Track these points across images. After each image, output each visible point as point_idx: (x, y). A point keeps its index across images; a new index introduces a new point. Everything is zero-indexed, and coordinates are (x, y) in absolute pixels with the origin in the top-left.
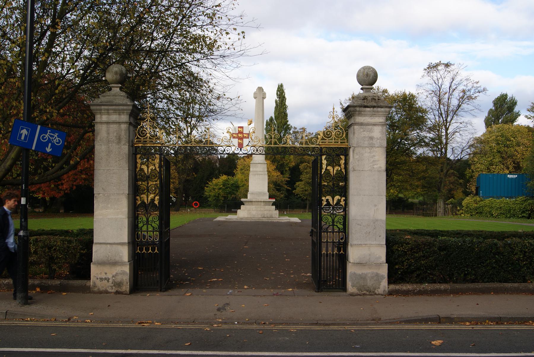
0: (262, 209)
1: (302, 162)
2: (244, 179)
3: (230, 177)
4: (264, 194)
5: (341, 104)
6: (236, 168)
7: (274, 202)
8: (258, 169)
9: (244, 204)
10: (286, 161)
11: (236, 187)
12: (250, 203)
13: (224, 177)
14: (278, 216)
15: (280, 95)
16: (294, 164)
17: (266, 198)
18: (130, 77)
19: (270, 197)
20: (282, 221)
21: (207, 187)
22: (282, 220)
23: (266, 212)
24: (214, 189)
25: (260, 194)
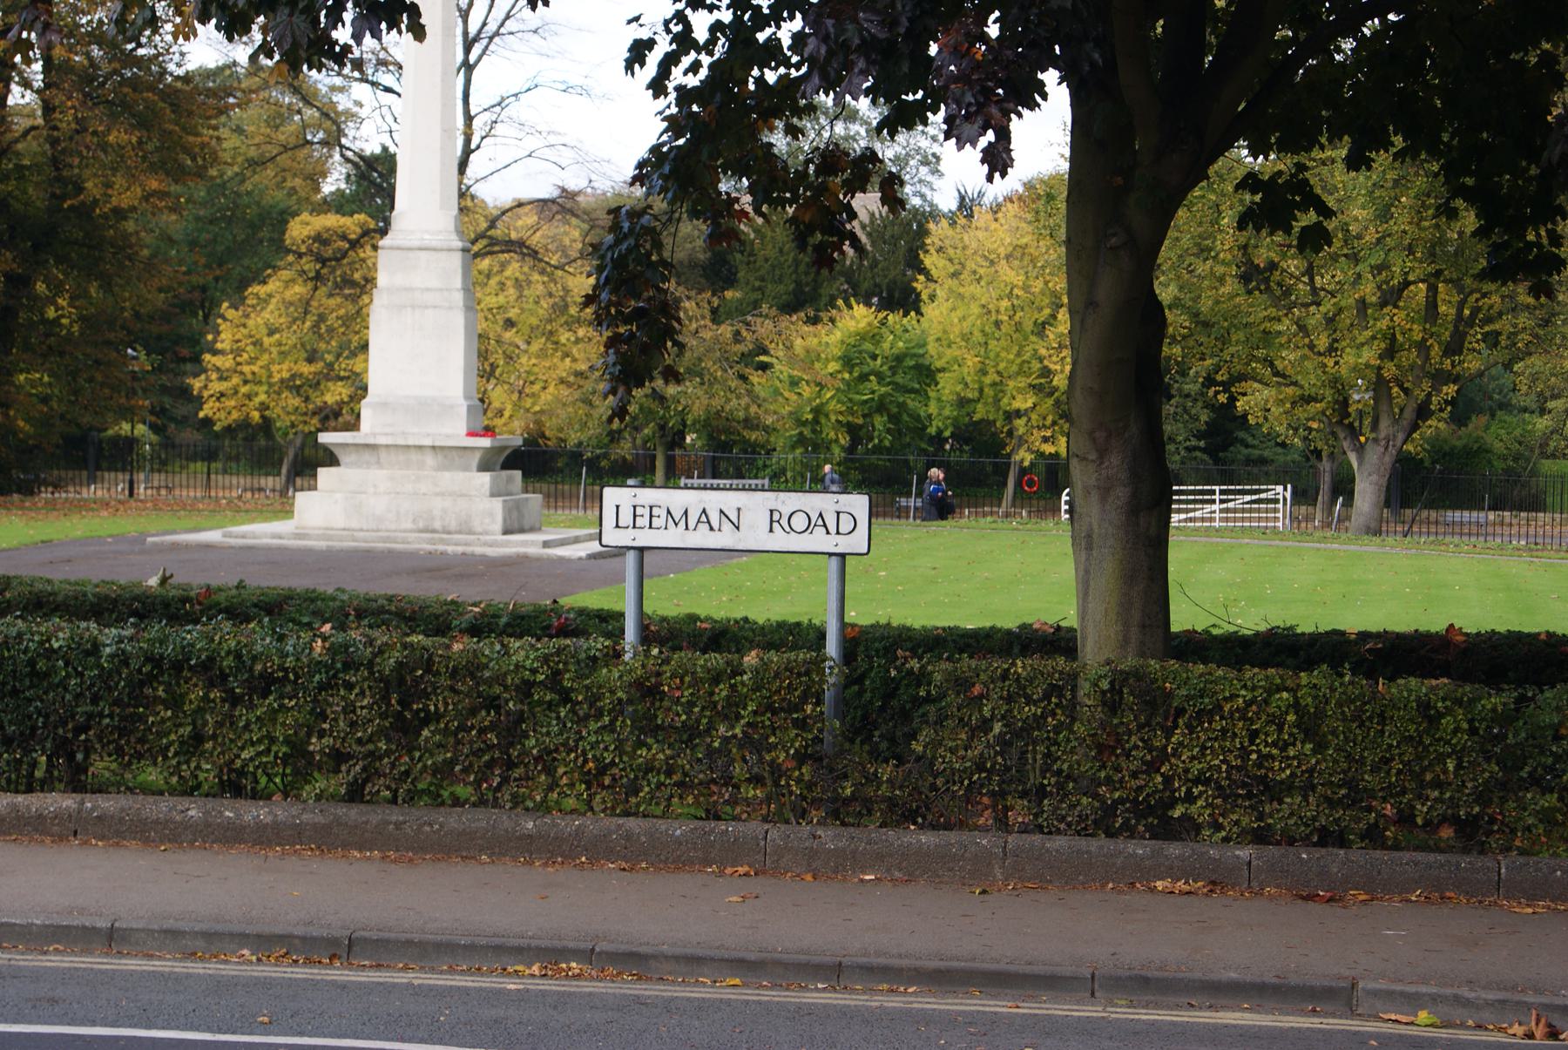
23: (438, 505)
25: (423, 408)
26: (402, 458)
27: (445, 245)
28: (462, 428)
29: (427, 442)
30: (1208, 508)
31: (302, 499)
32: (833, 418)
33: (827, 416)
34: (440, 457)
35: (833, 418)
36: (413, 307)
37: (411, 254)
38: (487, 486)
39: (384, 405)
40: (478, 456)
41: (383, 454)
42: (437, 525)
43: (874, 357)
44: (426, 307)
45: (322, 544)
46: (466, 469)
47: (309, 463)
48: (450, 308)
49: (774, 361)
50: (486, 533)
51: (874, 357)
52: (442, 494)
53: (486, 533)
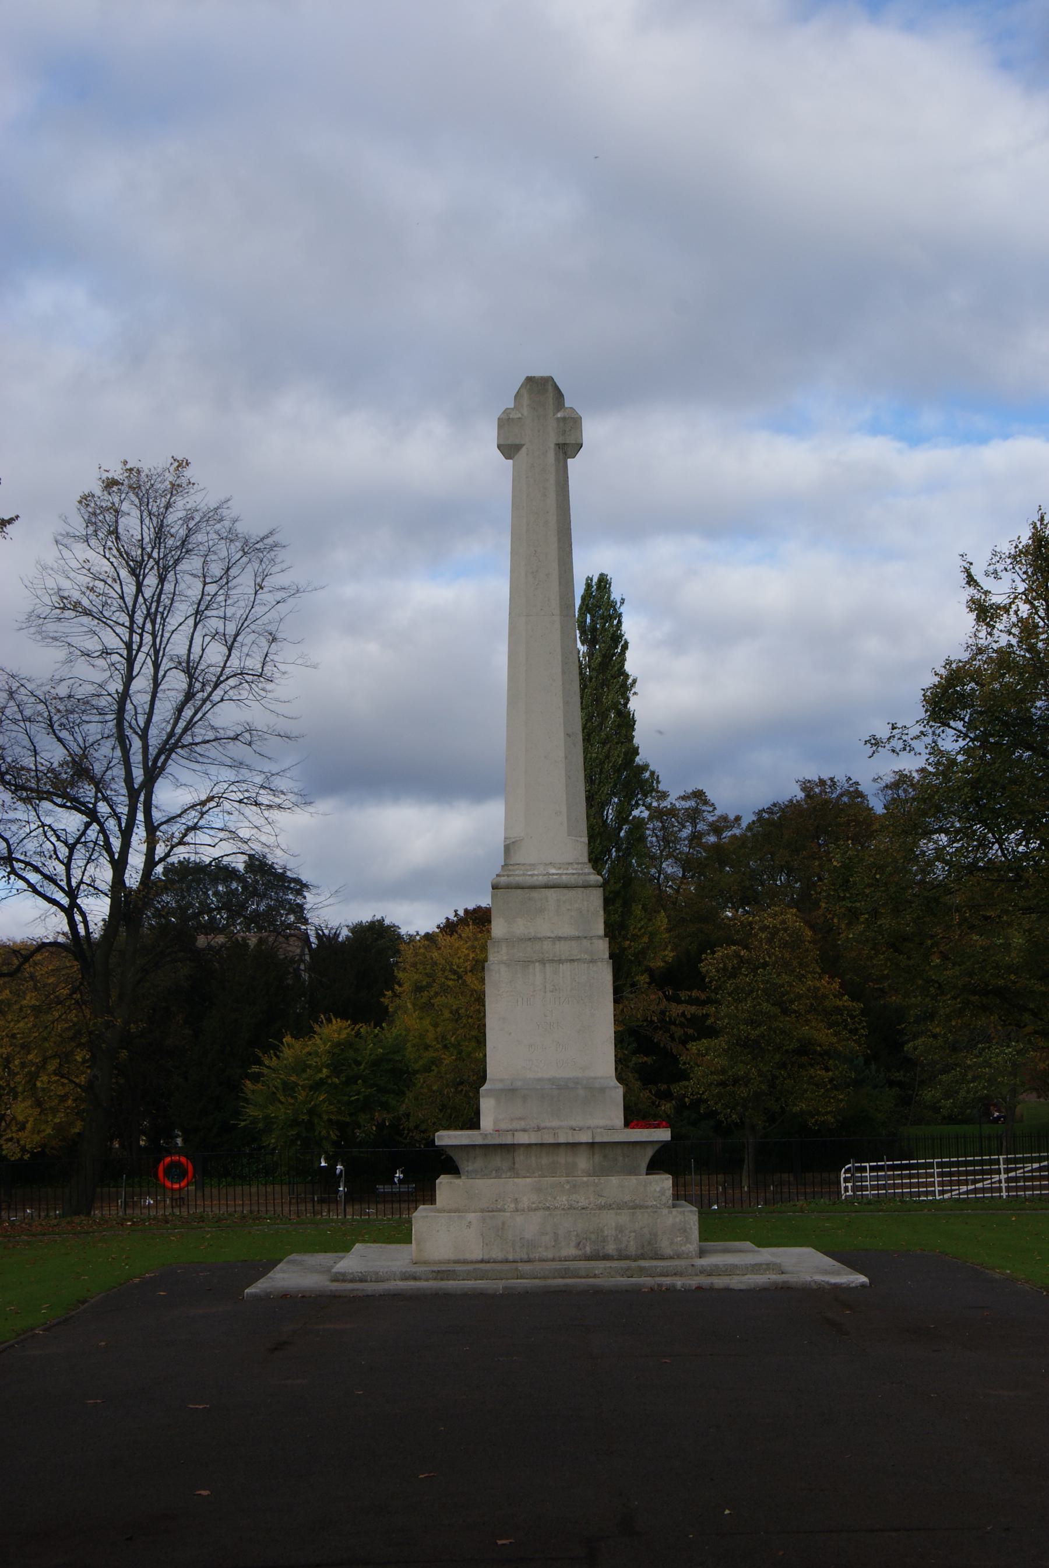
0: (581, 1200)
1: (709, 945)
2: (431, 1035)
3: (364, 1029)
4: (594, 1092)
5: (971, 581)
6: (390, 981)
7: (664, 1146)
8: (543, 927)
9: (454, 1170)
10: (635, 938)
11: (394, 1073)
12: (497, 1161)
13: (334, 1030)
14: (693, 1246)
15: (594, 629)
16: (670, 954)
17: (607, 1119)
18: (177, 902)
19: (633, 1116)
20: (735, 1282)
21: (256, 1078)
22: (729, 1270)
23: (610, 1221)
24: (289, 1088)
25: (564, 1092)
26: (545, 1161)
27: (580, 881)
28: (617, 1117)
29: (585, 1138)
30: (996, 1178)
31: (422, 1218)
32: (325, 1117)
33: (320, 1117)
34: (598, 1158)
35: (325, 1117)
36: (543, 962)
37: (535, 894)
38: (669, 1193)
39: (510, 1093)
40: (650, 1153)
41: (520, 1158)
42: (611, 1248)
43: (358, 1063)
44: (560, 961)
45: (497, 1286)
46: (633, 1171)
47: (429, 1168)
48: (593, 961)
49: (265, 1071)
50: (679, 1256)
51: (358, 1063)
52: (608, 1207)
53: (679, 1256)
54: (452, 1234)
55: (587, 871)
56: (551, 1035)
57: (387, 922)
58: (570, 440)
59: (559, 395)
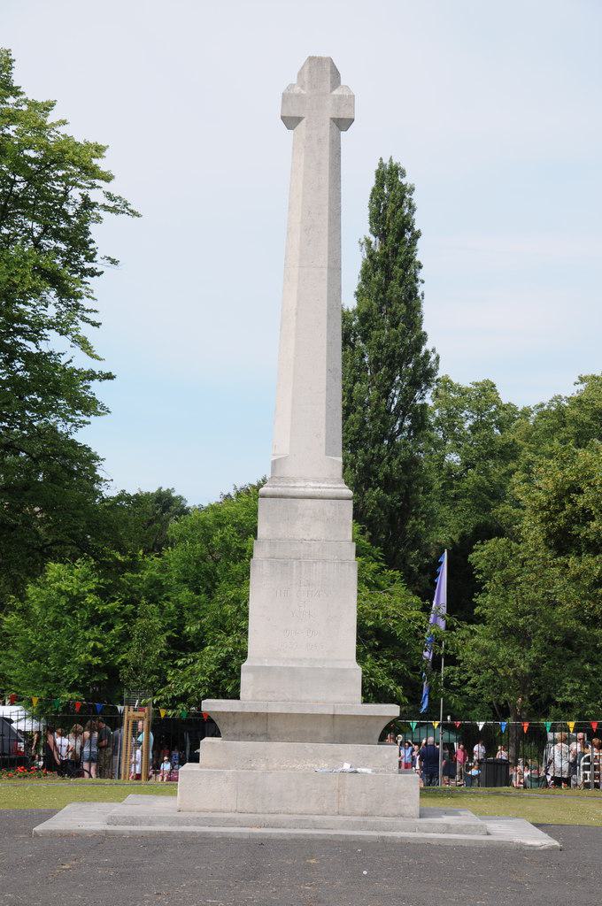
17: (346, 695)
19: (372, 693)
54: (215, 791)
55: (340, 486)
56: (303, 622)
57: (164, 489)
58: (343, 114)
59: (336, 74)
